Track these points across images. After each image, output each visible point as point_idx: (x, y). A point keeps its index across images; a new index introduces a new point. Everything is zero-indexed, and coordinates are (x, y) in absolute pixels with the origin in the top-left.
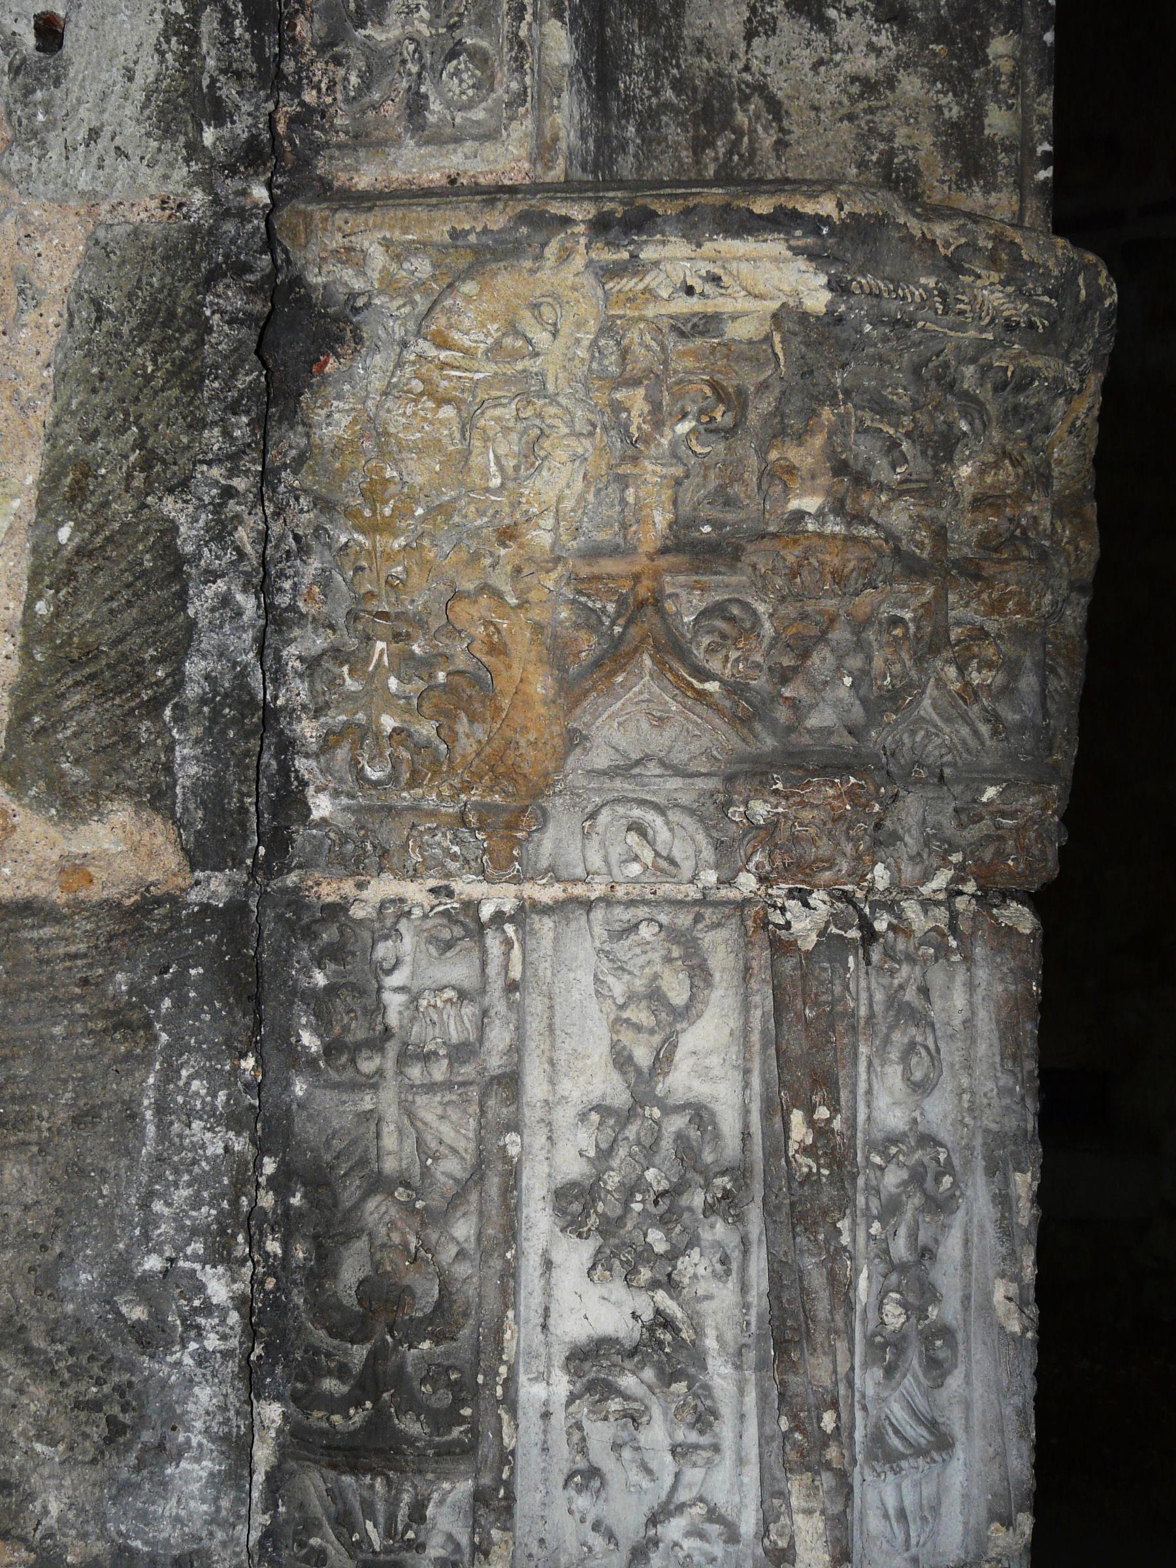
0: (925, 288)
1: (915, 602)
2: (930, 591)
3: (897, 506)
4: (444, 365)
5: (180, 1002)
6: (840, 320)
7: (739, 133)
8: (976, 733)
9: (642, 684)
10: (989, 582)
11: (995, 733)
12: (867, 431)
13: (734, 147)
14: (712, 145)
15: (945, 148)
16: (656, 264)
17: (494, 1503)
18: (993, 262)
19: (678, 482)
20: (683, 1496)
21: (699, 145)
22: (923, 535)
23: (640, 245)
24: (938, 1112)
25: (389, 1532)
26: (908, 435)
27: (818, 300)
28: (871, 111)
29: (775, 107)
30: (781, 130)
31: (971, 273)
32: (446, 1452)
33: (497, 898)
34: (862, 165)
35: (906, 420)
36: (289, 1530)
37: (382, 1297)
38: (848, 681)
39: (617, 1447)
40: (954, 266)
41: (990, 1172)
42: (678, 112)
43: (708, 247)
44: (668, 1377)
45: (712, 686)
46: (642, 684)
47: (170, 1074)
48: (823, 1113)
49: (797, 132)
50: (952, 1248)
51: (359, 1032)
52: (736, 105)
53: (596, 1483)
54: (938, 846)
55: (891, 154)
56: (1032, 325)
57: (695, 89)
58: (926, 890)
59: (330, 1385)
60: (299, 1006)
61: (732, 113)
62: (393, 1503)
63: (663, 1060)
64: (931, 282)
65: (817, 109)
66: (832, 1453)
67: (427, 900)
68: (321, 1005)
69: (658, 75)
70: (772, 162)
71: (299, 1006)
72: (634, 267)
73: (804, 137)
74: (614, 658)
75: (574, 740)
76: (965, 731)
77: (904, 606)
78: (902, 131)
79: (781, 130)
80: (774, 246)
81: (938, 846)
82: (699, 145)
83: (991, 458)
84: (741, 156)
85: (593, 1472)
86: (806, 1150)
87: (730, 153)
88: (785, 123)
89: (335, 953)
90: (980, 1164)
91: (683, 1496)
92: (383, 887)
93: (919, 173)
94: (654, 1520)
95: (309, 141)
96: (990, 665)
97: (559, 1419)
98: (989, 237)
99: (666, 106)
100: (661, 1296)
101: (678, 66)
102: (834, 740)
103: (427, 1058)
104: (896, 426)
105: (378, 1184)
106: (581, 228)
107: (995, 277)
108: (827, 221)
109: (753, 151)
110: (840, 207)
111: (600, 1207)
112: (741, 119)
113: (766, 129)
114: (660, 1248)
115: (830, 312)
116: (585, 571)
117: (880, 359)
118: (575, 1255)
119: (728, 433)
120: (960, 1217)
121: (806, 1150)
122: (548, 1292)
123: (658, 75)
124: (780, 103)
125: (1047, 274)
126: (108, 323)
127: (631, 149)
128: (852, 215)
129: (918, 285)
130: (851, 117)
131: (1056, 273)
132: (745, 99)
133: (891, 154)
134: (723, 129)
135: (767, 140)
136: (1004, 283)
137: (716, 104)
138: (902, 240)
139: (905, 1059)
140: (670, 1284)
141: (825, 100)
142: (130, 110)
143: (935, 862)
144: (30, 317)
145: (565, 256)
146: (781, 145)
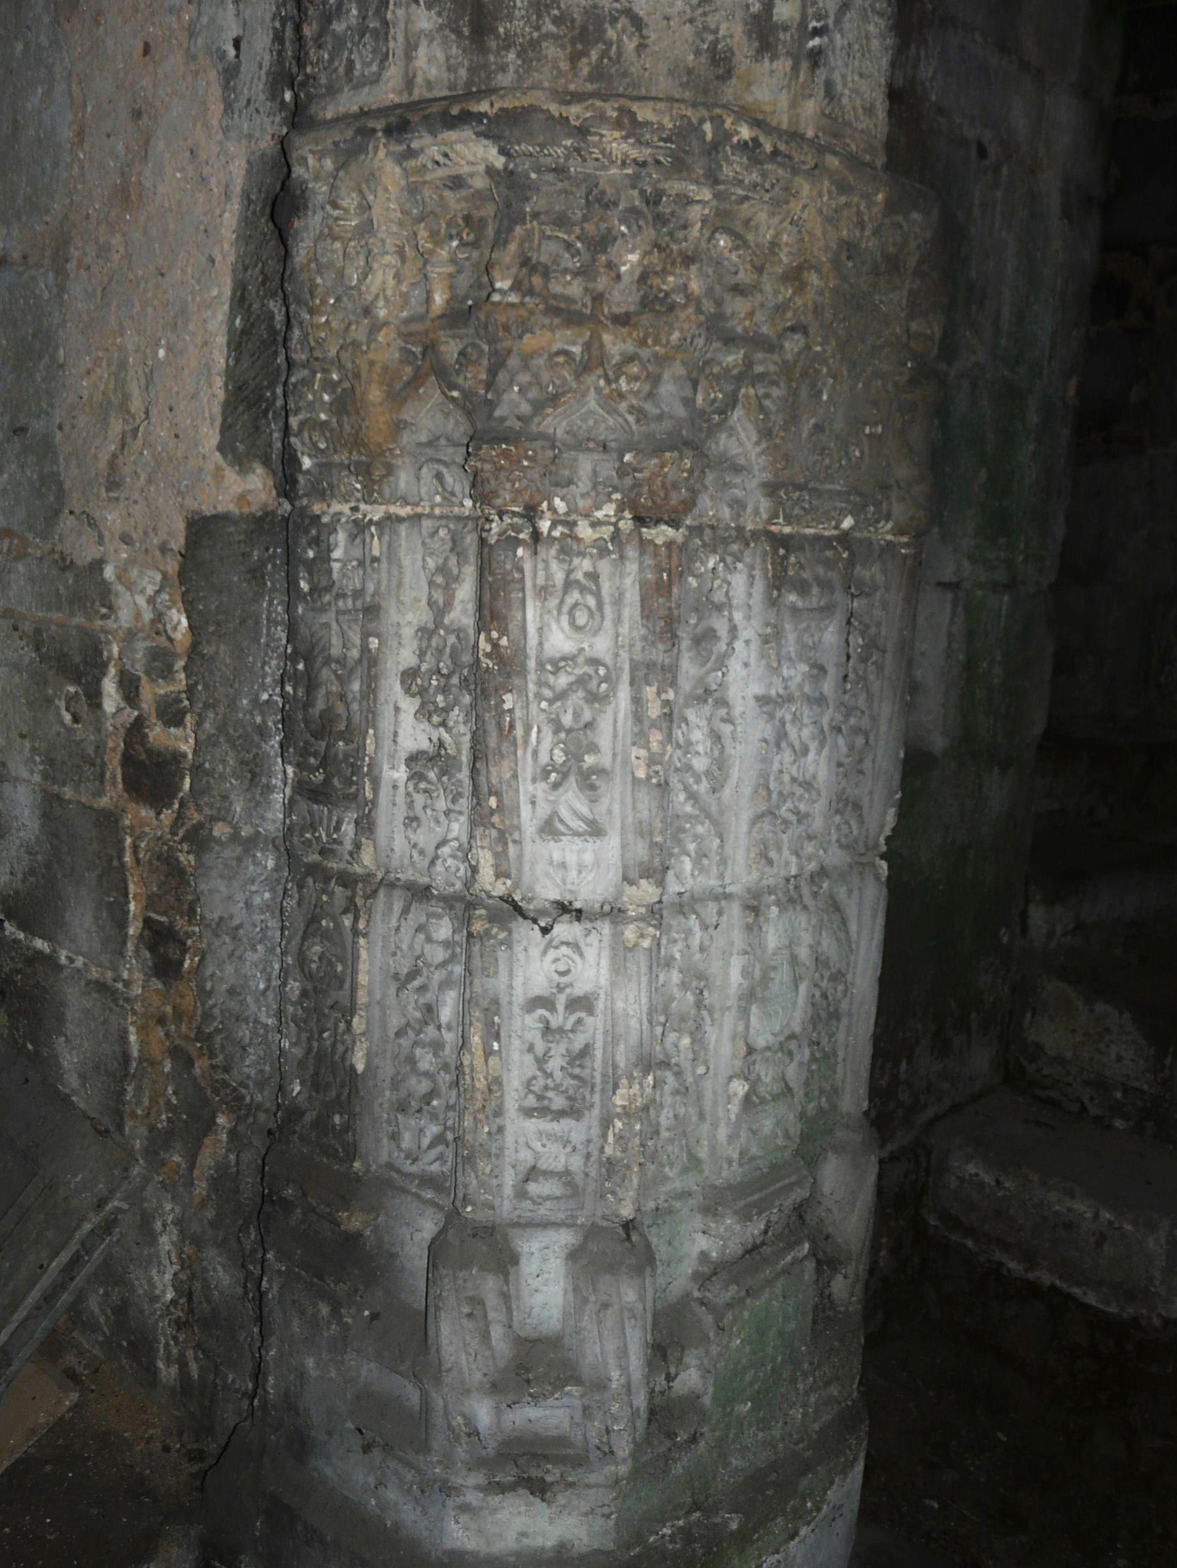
0: (566, 147)
1: (580, 341)
2: (588, 334)
3: (576, 283)
4: (337, 219)
5: (274, 566)
6: (512, 173)
7: (609, 44)
8: (626, 421)
9: (432, 392)
10: (635, 326)
11: (638, 421)
12: (549, 237)
13: (604, 54)
14: (587, 55)
15: (749, 34)
16: (422, 150)
17: (366, 825)
18: (618, 124)
19: (451, 276)
20: (450, 836)
21: (574, 58)
22: (588, 300)
23: (411, 140)
24: (601, 646)
25: (329, 835)
26: (578, 238)
27: (499, 162)
28: (705, 14)
29: (638, 23)
30: (642, 37)
31: (596, 134)
32: (346, 797)
33: (376, 513)
34: (697, 52)
35: (577, 230)
36: (297, 828)
37: (327, 720)
38: (516, 389)
39: (425, 807)
40: (582, 132)
41: (632, 684)
42: (556, 37)
43: (440, 136)
44: (443, 772)
45: (455, 394)
46: (432, 392)
47: (271, 603)
48: (495, 635)
49: (653, 36)
50: (605, 725)
51: (324, 583)
52: (607, 26)
53: (415, 824)
54: (600, 490)
55: (716, 42)
56: (658, 162)
57: (573, 21)
58: (599, 514)
59: (312, 760)
60: (301, 568)
61: (604, 31)
62: (330, 819)
63: (449, 604)
64: (568, 143)
65: (668, 19)
66: (496, 819)
67: (348, 512)
68: (310, 565)
69: (539, 17)
70: (635, 59)
71: (301, 568)
72: (411, 154)
73: (659, 39)
74: (416, 381)
75: (398, 427)
76: (620, 420)
77: (574, 343)
78: (724, 27)
79: (642, 37)
80: (467, 133)
81: (600, 490)
82: (574, 58)
83: (648, 248)
84: (610, 59)
85: (416, 818)
86: (487, 655)
87: (601, 58)
88: (645, 32)
89: (316, 542)
90: (626, 677)
91: (450, 836)
92: (336, 507)
93: (733, 53)
94: (437, 847)
95: (308, 95)
96: (636, 378)
97: (402, 790)
98: (614, 109)
99: (549, 36)
100: (442, 729)
101: (559, 8)
102: (508, 423)
103: (344, 596)
104: (569, 233)
105: (328, 660)
106: (380, 134)
107: (617, 134)
108: (485, 115)
109: (620, 53)
110: (492, 105)
111: (419, 681)
112: (611, 33)
113: (630, 38)
114: (441, 705)
115: (506, 168)
116: (405, 330)
117: (566, 192)
118: (410, 706)
119: (475, 245)
120: (610, 709)
121: (487, 655)
122: (397, 723)
123: (539, 17)
124: (641, 19)
125: (662, 127)
126: (252, 207)
127: (512, 68)
128: (502, 110)
129: (559, 146)
130: (691, 21)
131: (670, 126)
132: (614, 20)
133: (716, 42)
134: (597, 42)
135: (630, 45)
136: (624, 138)
137: (591, 28)
138: (547, 119)
139: (571, 612)
140: (443, 724)
141: (673, 12)
142: (261, 87)
143: (602, 497)
144: (228, 207)
145: (376, 148)
146: (641, 47)
